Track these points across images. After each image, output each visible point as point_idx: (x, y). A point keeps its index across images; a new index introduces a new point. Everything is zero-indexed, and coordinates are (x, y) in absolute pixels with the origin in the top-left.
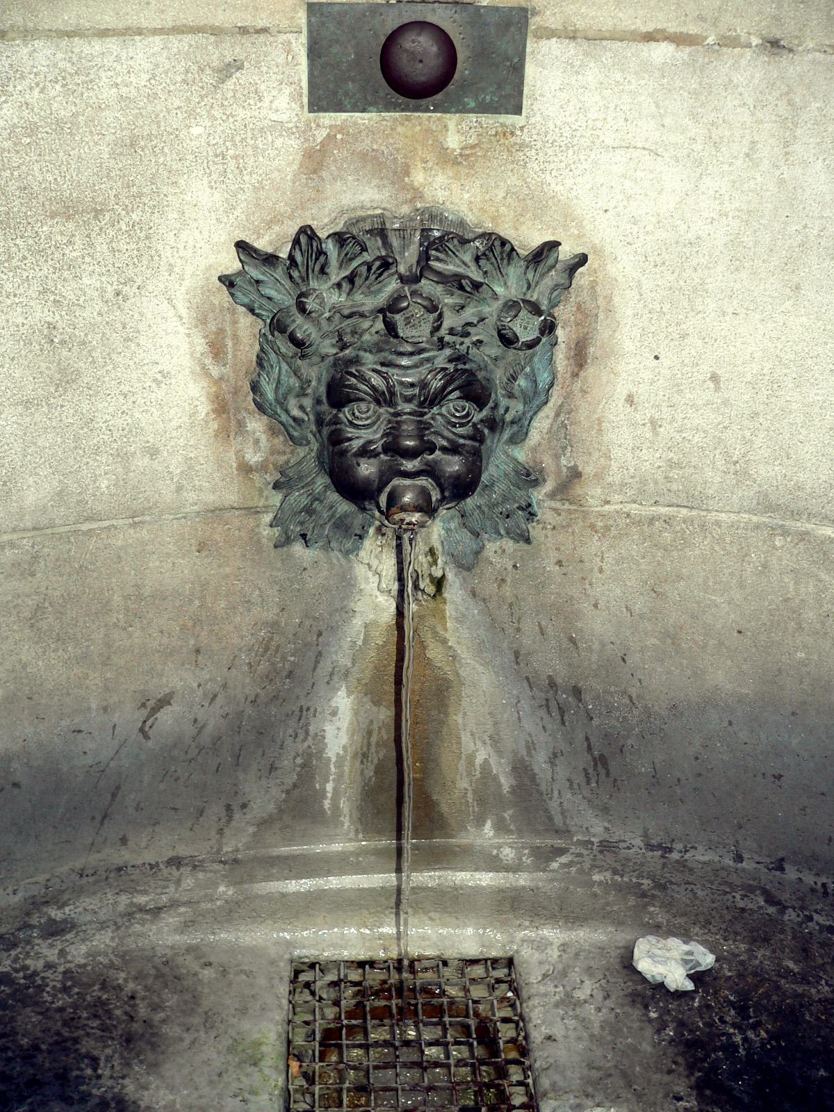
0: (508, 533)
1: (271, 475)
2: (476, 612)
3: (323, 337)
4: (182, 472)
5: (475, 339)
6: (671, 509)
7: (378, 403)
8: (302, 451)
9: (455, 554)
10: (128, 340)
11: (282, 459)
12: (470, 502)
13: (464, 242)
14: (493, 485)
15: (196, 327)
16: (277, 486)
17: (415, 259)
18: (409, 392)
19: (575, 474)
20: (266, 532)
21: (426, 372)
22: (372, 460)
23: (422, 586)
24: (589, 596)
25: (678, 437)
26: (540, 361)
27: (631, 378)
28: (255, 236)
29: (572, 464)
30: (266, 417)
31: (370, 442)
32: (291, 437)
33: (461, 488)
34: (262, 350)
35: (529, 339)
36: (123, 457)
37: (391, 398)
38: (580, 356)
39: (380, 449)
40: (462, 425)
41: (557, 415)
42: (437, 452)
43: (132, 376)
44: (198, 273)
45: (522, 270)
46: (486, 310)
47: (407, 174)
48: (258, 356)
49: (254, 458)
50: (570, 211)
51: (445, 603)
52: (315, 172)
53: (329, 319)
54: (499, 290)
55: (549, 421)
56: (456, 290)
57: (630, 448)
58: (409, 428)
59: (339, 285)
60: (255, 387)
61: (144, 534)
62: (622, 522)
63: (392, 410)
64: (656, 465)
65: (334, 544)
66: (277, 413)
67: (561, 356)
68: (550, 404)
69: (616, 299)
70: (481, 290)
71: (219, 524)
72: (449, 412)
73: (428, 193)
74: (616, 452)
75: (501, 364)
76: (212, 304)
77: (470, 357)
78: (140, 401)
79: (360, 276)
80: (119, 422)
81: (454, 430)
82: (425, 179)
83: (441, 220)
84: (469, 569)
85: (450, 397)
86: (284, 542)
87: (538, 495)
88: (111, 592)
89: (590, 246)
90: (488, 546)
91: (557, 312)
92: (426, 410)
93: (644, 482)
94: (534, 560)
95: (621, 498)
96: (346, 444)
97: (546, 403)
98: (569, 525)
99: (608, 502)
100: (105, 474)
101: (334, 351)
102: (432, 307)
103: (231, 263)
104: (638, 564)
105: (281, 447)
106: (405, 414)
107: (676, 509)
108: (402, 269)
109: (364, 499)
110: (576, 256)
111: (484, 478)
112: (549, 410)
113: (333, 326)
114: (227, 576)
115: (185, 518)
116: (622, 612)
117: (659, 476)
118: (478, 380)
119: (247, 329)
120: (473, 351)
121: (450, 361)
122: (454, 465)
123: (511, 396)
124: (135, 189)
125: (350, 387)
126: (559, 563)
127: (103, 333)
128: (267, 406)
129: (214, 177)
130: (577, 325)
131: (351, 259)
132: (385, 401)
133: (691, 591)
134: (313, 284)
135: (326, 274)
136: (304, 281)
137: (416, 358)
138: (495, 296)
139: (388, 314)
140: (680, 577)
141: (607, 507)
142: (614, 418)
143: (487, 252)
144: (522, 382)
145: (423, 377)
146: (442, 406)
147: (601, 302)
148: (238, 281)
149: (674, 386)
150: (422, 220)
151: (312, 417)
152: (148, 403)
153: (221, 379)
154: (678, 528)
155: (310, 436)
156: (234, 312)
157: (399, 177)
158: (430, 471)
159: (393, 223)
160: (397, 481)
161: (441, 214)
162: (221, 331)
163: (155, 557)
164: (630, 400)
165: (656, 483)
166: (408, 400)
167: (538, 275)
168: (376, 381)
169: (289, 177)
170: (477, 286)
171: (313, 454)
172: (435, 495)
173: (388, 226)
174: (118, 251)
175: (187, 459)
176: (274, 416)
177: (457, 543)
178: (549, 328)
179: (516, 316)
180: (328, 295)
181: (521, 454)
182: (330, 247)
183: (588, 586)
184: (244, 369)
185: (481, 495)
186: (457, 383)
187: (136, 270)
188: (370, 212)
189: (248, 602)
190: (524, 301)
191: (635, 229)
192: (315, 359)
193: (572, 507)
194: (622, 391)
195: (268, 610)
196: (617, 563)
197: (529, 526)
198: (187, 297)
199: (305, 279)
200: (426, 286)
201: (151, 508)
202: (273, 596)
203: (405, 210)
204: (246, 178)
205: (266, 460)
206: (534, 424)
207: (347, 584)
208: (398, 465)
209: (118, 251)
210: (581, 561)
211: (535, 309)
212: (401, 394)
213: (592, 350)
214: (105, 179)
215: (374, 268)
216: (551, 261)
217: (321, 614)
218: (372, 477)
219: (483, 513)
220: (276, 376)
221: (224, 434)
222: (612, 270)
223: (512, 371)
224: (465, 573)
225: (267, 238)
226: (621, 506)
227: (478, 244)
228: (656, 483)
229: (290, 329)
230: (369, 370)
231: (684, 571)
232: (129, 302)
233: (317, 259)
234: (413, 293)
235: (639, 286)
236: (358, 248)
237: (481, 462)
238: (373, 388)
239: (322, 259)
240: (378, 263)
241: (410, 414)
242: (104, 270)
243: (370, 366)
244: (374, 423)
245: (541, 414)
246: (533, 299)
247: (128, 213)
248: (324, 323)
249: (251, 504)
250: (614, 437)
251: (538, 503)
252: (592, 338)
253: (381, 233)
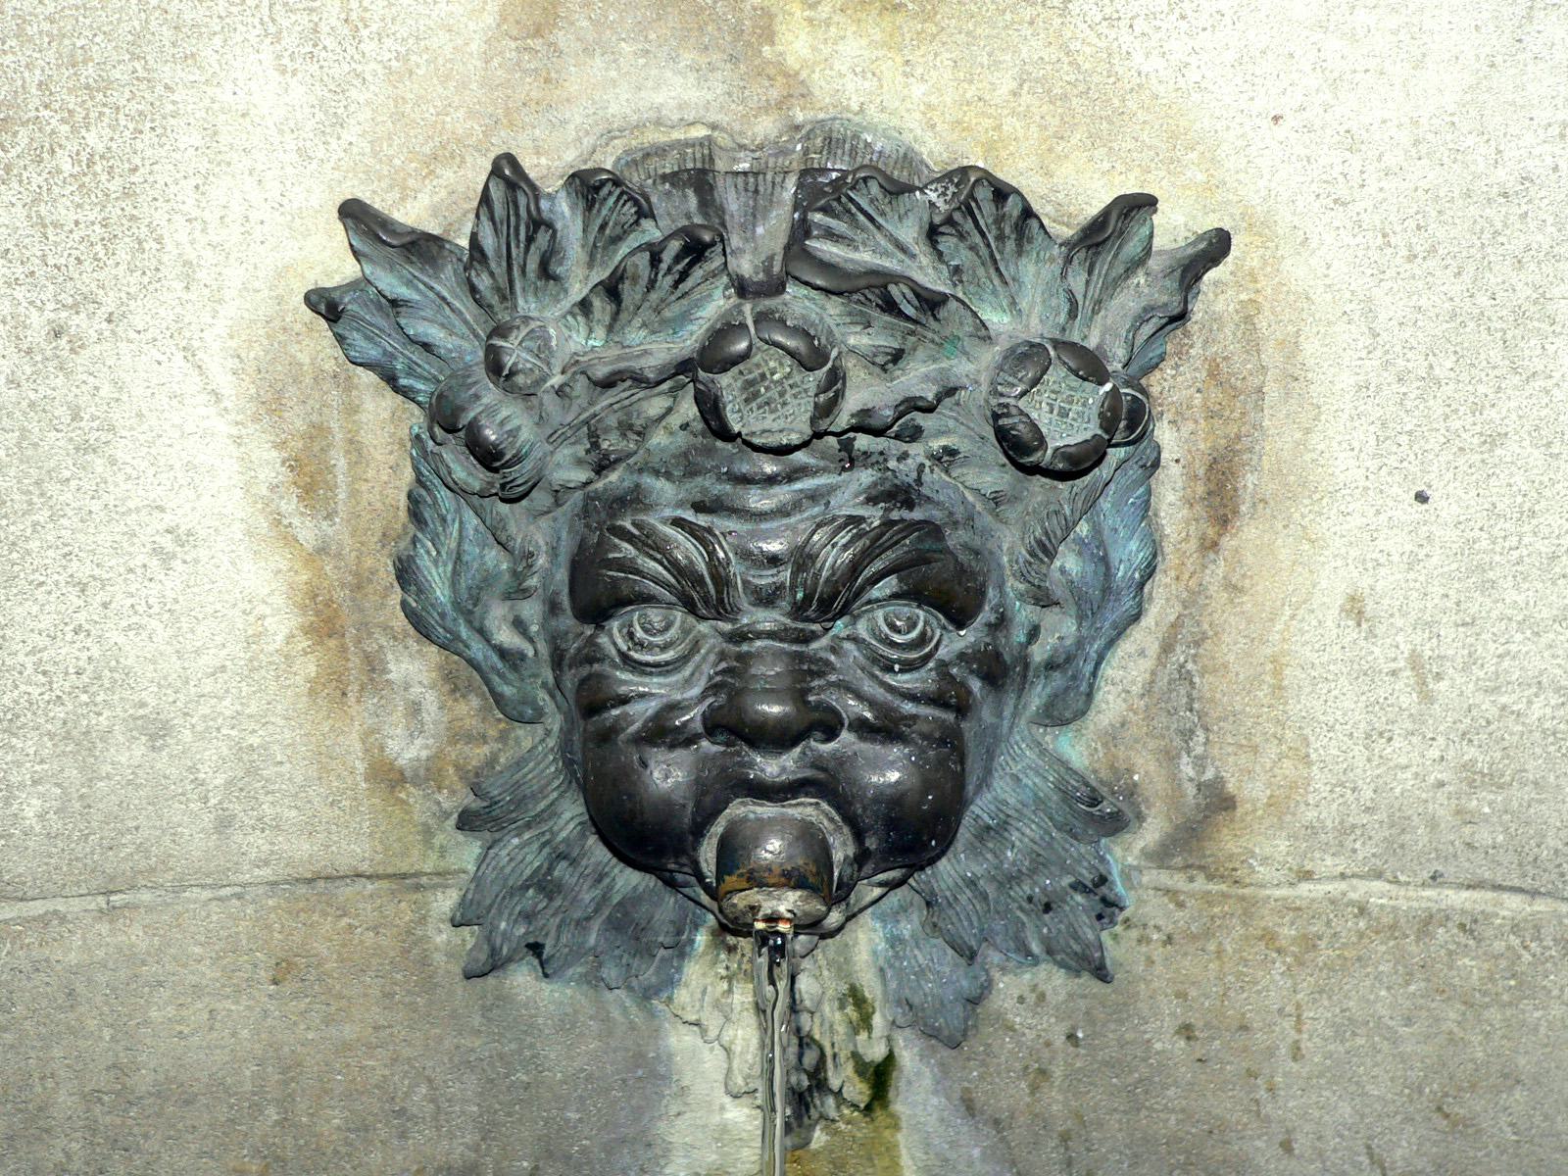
0: (1049, 952)
1: (453, 792)
2: (976, 1152)
3: (555, 438)
4: (229, 783)
5: (936, 445)
6: (1476, 895)
7: (690, 607)
8: (526, 737)
9: (916, 1000)
10: (85, 448)
11: (478, 753)
12: (947, 871)
13: (896, 190)
14: (1004, 825)
15: (256, 419)
16: (467, 822)
17: (782, 240)
18: (765, 579)
19: (1219, 802)
20: (443, 936)
21: (809, 526)
22: (680, 754)
23: (834, 1082)
24: (1268, 1120)
25: (1487, 706)
26: (1117, 506)
27: (1354, 553)
28: (396, 194)
29: (1209, 774)
30: (434, 649)
31: (674, 708)
32: (499, 699)
33: (910, 836)
34: (420, 480)
35: (1072, 441)
36: (79, 741)
37: (719, 592)
38: (1220, 497)
39: (698, 726)
40: (909, 667)
41: (1167, 648)
42: (846, 736)
43: (99, 538)
44: (257, 285)
45: (1057, 268)
46: (961, 368)
47: (769, 36)
48: (409, 496)
49: (408, 750)
50: (1183, 123)
51: (896, 1127)
52: (538, 32)
53: (560, 392)
54: (996, 319)
55: (1147, 664)
56: (876, 313)
57: (1359, 734)
58: (769, 670)
59: (584, 306)
60: (405, 573)
61: (136, 935)
62: (1349, 926)
63: (727, 627)
64: (1431, 779)
65: (611, 972)
66: (457, 637)
67: (1171, 497)
68: (1148, 621)
69: (1310, 348)
70: (942, 313)
71: (325, 914)
72: (875, 632)
73: (822, 85)
74: (1324, 747)
75: (1011, 513)
76: (295, 363)
77: (925, 490)
78: (121, 602)
79: (635, 279)
80: (67, 652)
81: (888, 679)
82: (814, 49)
83: (854, 149)
84: (957, 1046)
85: (876, 592)
86: (489, 965)
87: (1124, 854)
88: (50, 1083)
89: (1237, 211)
90: (1002, 983)
91: (1155, 383)
92: (816, 627)
93: (1399, 824)
94: (1121, 1022)
95: (1341, 865)
96: (615, 712)
97: (1136, 618)
98: (1207, 934)
99: (1307, 876)
100: (35, 783)
101: (581, 475)
102: (812, 357)
103: (334, 261)
104: (1395, 1040)
105: (472, 723)
106: (759, 635)
107: (1490, 895)
108: (746, 266)
109: (661, 851)
110: (1200, 238)
111: (980, 809)
112: (1144, 637)
113: (575, 409)
114: (345, 1048)
115: (239, 897)
116: (1356, 1165)
117: (1443, 812)
118: (947, 551)
119: (383, 423)
120: (934, 477)
121: (872, 500)
122: (888, 771)
123: (1043, 599)
124: (89, 72)
125: (623, 565)
126: (1187, 1031)
127: (23, 429)
128: (433, 619)
129: (289, 41)
130: (1211, 415)
131: (616, 240)
132: (706, 601)
133: (1546, 1117)
134: (526, 304)
135: (556, 278)
136: (503, 298)
137: (783, 493)
138: (983, 333)
139: (701, 374)
140: (1511, 1079)
141: (1304, 888)
142: (1313, 657)
143: (957, 216)
144: (1069, 562)
145: (800, 540)
146: (856, 618)
147: (1271, 355)
148: (350, 304)
149: (1470, 572)
150: (806, 151)
151: (543, 648)
152: (140, 609)
153: (322, 550)
154: (1499, 946)
155: (543, 697)
156: (349, 386)
157: (749, 44)
158: (824, 784)
159: (735, 160)
160: (741, 809)
161: (856, 136)
162: (318, 432)
163: (165, 993)
164: (1355, 609)
165: (1433, 824)
166: (766, 599)
167: (1097, 282)
168: (686, 548)
169: (474, 47)
170: (931, 303)
171: (551, 742)
172: (842, 850)
173: (720, 165)
174: (55, 225)
175: (241, 750)
176: (450, 645)
177: (921, 973)
178: (1128, 420)
179: (1036, 382)
180: (562, 334)
181: (1076, 748)
182: (565, 212)
183: (1262, 1094)
184: (378, 526)
185: (974, 851)
186: (890, 556)
187: (101, 275)
188: (678, 135)
189: (402, 1112)
190: (1056, 343)
191: (1356, 162)
192: (540, 498)
193: (1213, 887)
194: (1333, 585)
195: (452, 1136)
196: (1339, 1035)
197: (1105, 936)
198: (233, 344)
199: (507, 295)
200: (798, 302)
201: (153, 870)
202: (465, 1101)
203: (766, 127)
204: (368, 47)
205: (438, 756)
206: (1108, 671)
207: (649, 1076)
208: (742, 765)
209: (55, 225)
210: (1244, 1028)
211: (1091, 367)
212: (745, 583)
213: (1250, 479)
214: (13, 43)
215: (667, 257)
216: (1132, 248)
217: (584, 1151)
218: (677, 798)
219: (985, 897)
220: (453, 545)
221: (333, 689)
222: (1297, 271)
223: (1039, 532)
224: (946, 1053)
225: (425, 199)
226: (1343, 886)
227: (933, 196)
228: (1433, 824)
229: (463, 421)
230: (664, 521)
231: (1522, 1061)
232: (85, 353)
233: (530, 240)
234: (761, 318)
235: (1369, 312)
236: (630, 210)
237: (962, 761)
238: (673, 566)
239: (543, 238)
240: (675, 246)
241: (771, 635)
242: (19, 271)
243: (668, 513)
244: (684, 659)
245: (1126, 646)
246: (1092, 343)
247: (74, 130)
248: (550, 402)
249: (404, 867)
250: (1318, 704)
251: (1126, 875)
252: (1251, 450)
253: (700, 180)
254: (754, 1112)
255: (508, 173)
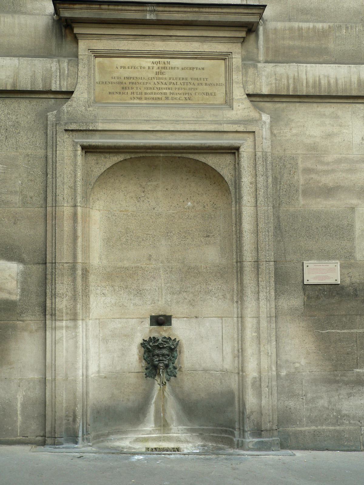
19: (181, 367)
36: (128, 364)
38: (180, 352)
60: (144, 356)
87: (176, 370)
112: (177, 359)
254: (72, 208)
255: (150, 337)
